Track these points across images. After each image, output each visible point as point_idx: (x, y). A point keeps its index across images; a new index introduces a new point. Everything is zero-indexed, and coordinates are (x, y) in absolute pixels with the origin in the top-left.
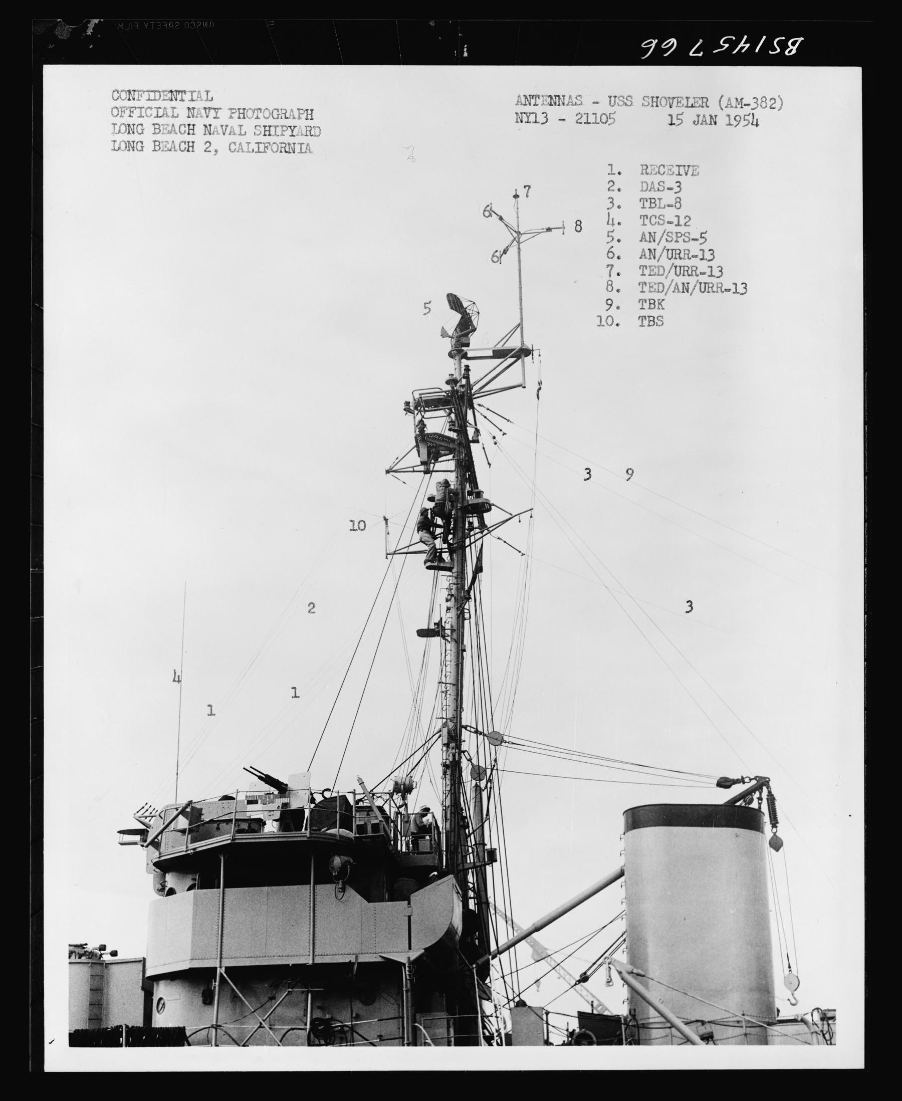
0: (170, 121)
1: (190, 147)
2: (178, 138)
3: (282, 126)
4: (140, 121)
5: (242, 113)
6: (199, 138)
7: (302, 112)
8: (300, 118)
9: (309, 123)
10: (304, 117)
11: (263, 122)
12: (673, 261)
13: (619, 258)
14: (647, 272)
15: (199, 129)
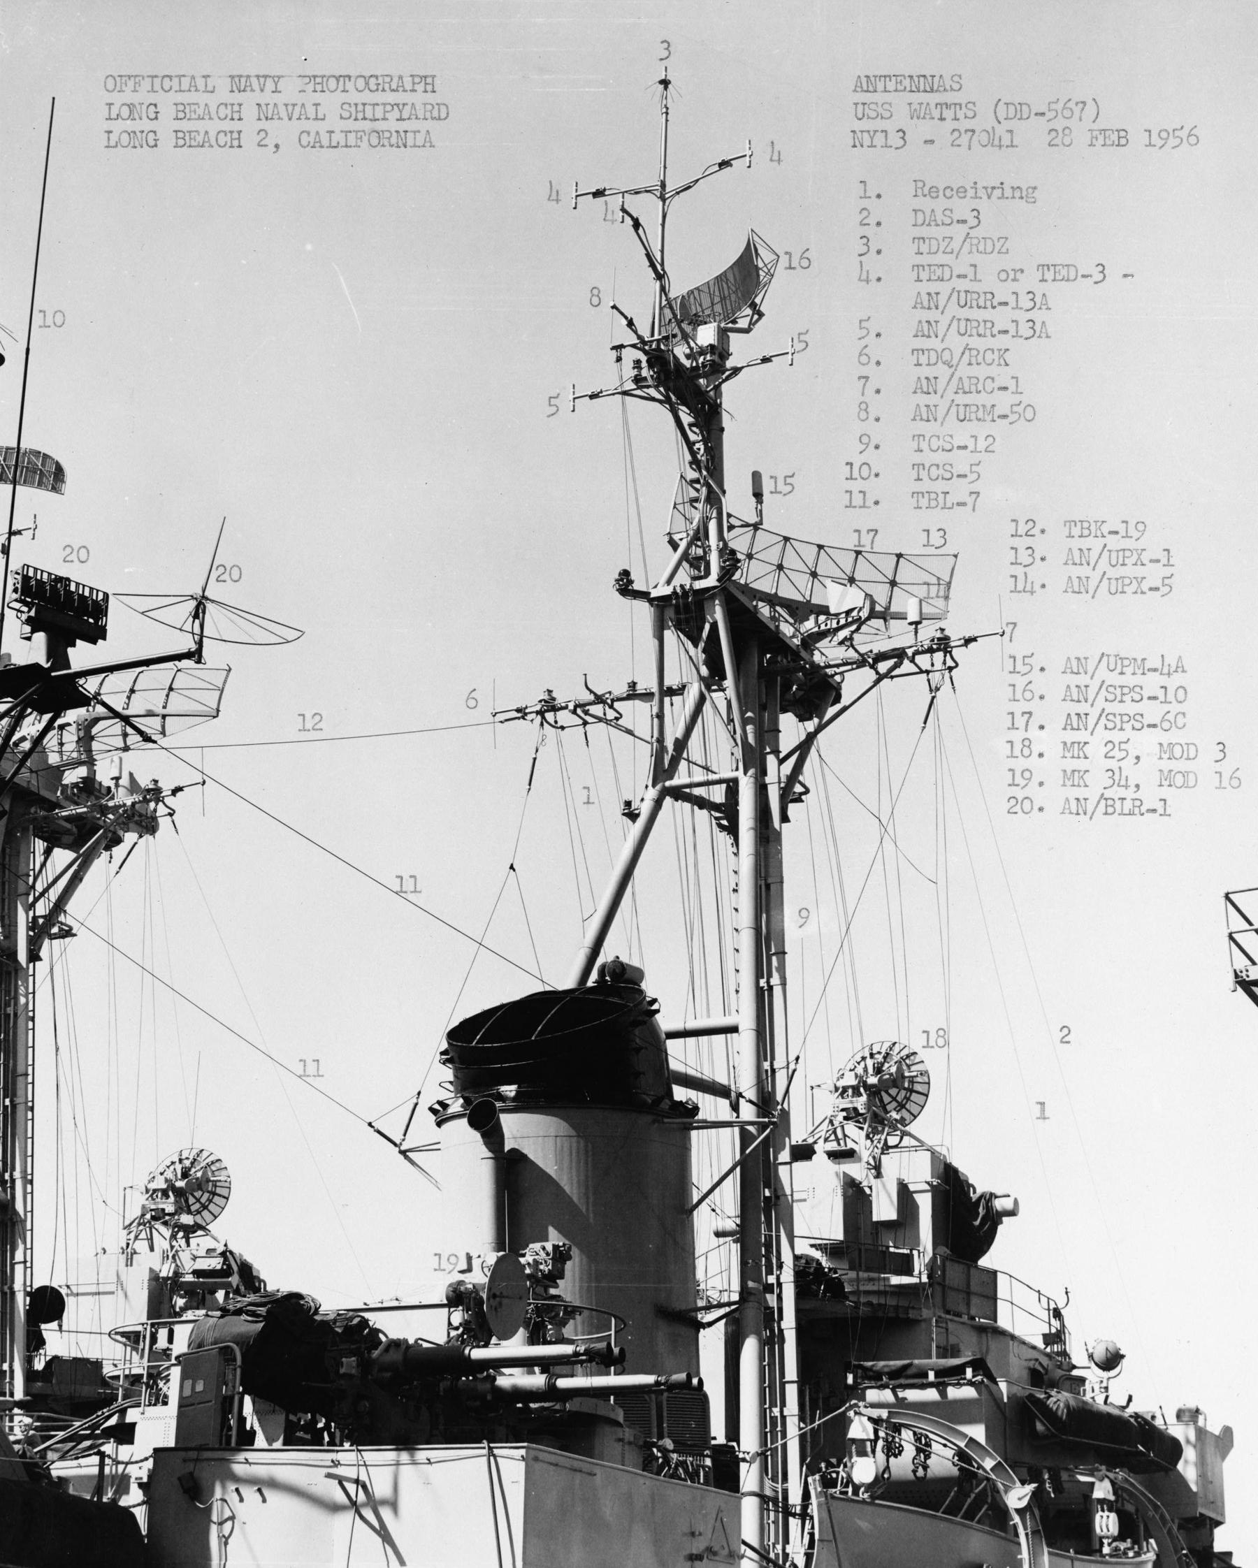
0: (202, 98)
1: (235, 141)
2: (213, 127)
3: (384, 104)
4: (152, 98)
5: (317, 81)
6: (250, 126)
7: (417, 80)
8: (413, 90)
9: (430, 98)
10: (420, 88)
11: (354, 97)
12: (966, 339)
13: (878, 363)
14: (924, 276)
15: (250, 112)
